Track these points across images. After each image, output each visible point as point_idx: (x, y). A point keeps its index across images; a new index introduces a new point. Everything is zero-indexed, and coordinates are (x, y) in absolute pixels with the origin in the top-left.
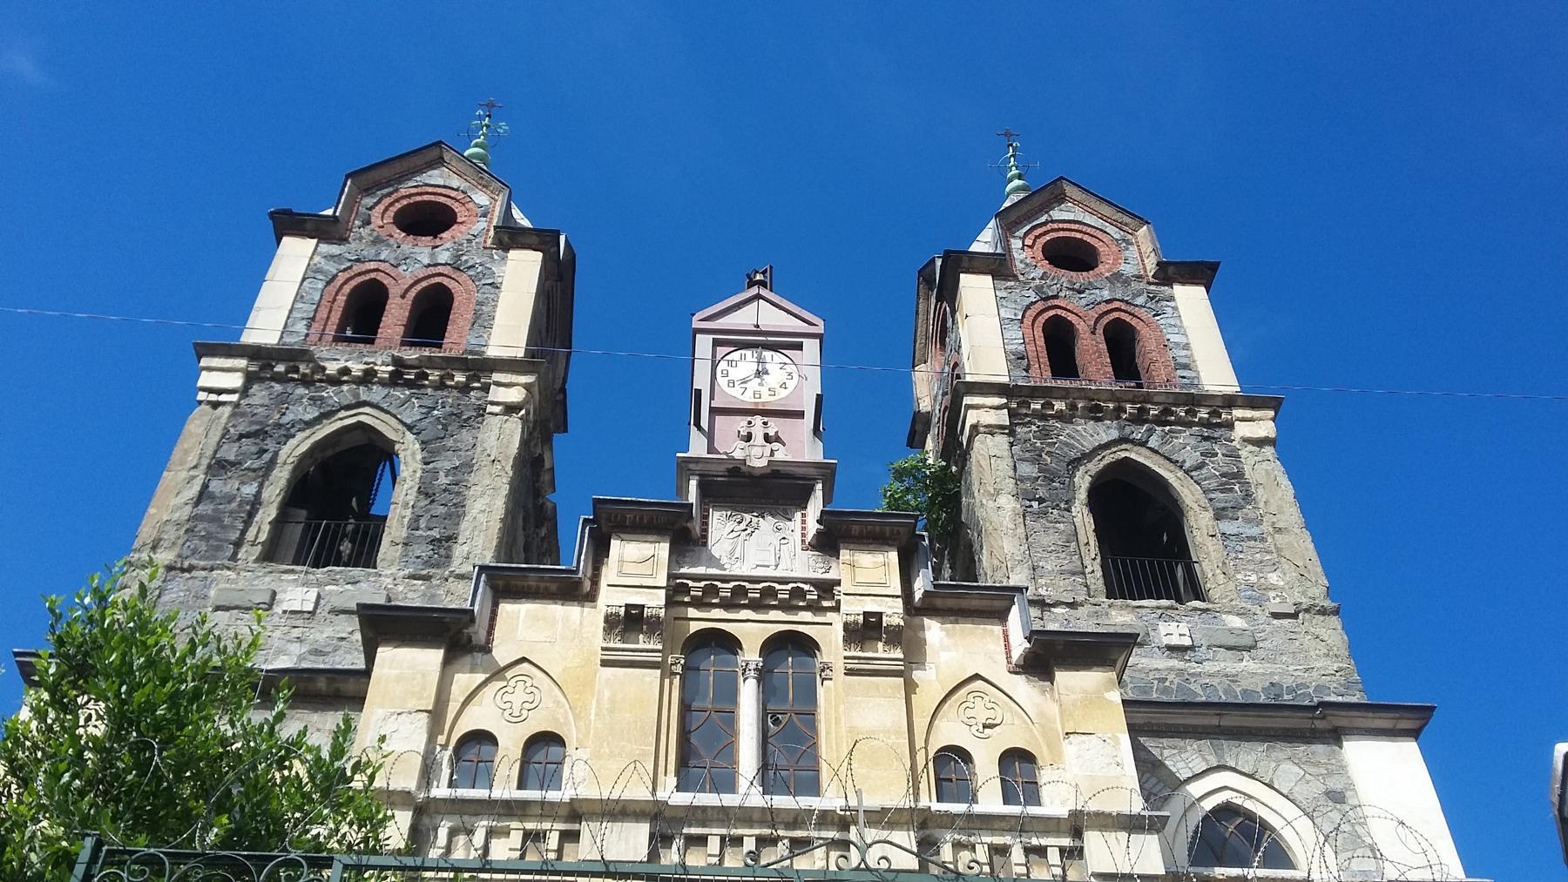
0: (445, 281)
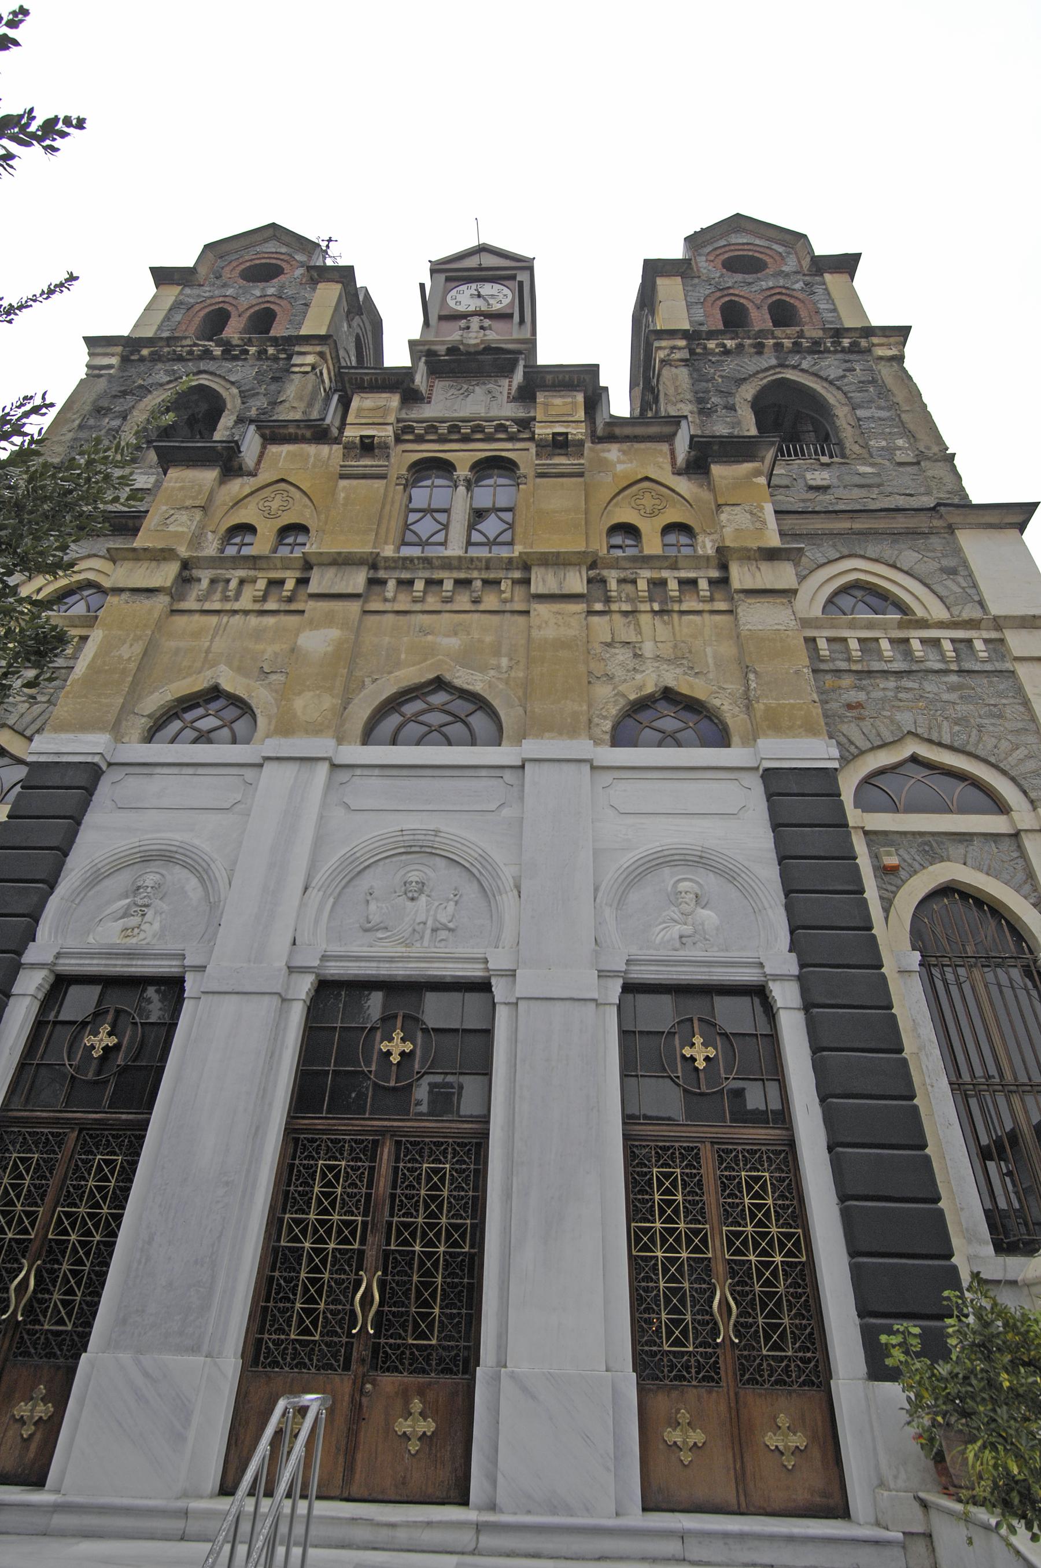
0: (272, 306)
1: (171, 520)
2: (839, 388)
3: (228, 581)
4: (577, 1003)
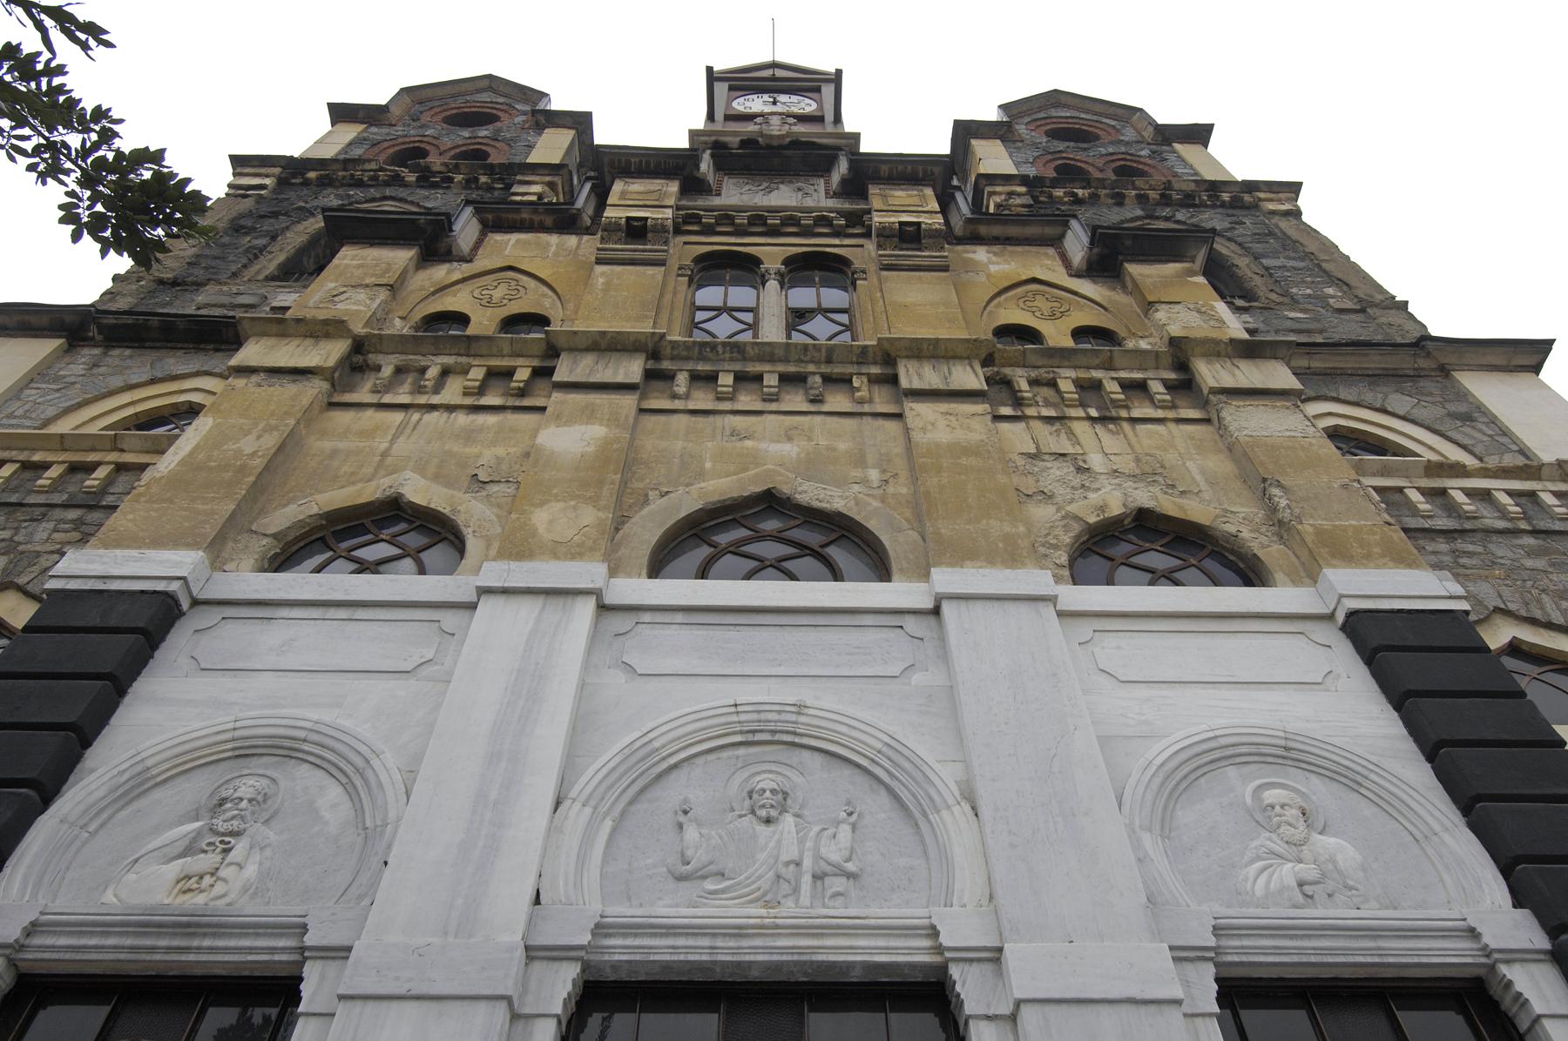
1: (342, 297)
2: (1229, 239)
3: (423, 370)
4: (1143, 1009)
